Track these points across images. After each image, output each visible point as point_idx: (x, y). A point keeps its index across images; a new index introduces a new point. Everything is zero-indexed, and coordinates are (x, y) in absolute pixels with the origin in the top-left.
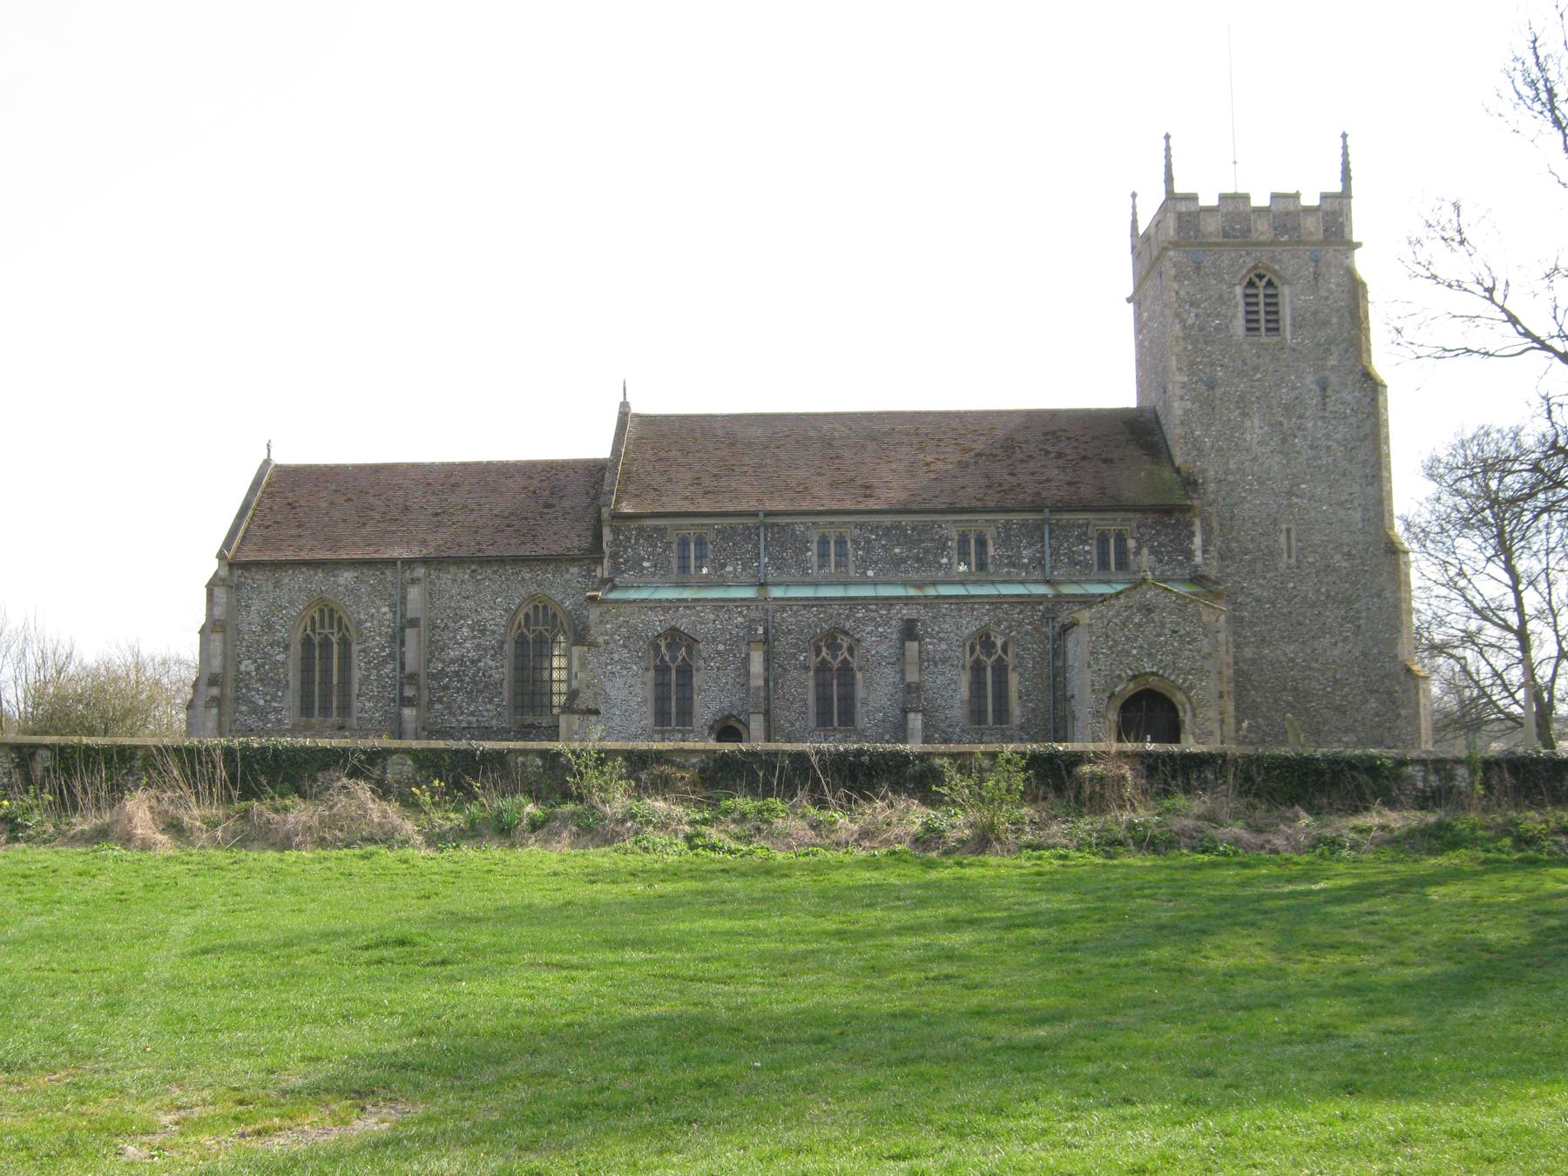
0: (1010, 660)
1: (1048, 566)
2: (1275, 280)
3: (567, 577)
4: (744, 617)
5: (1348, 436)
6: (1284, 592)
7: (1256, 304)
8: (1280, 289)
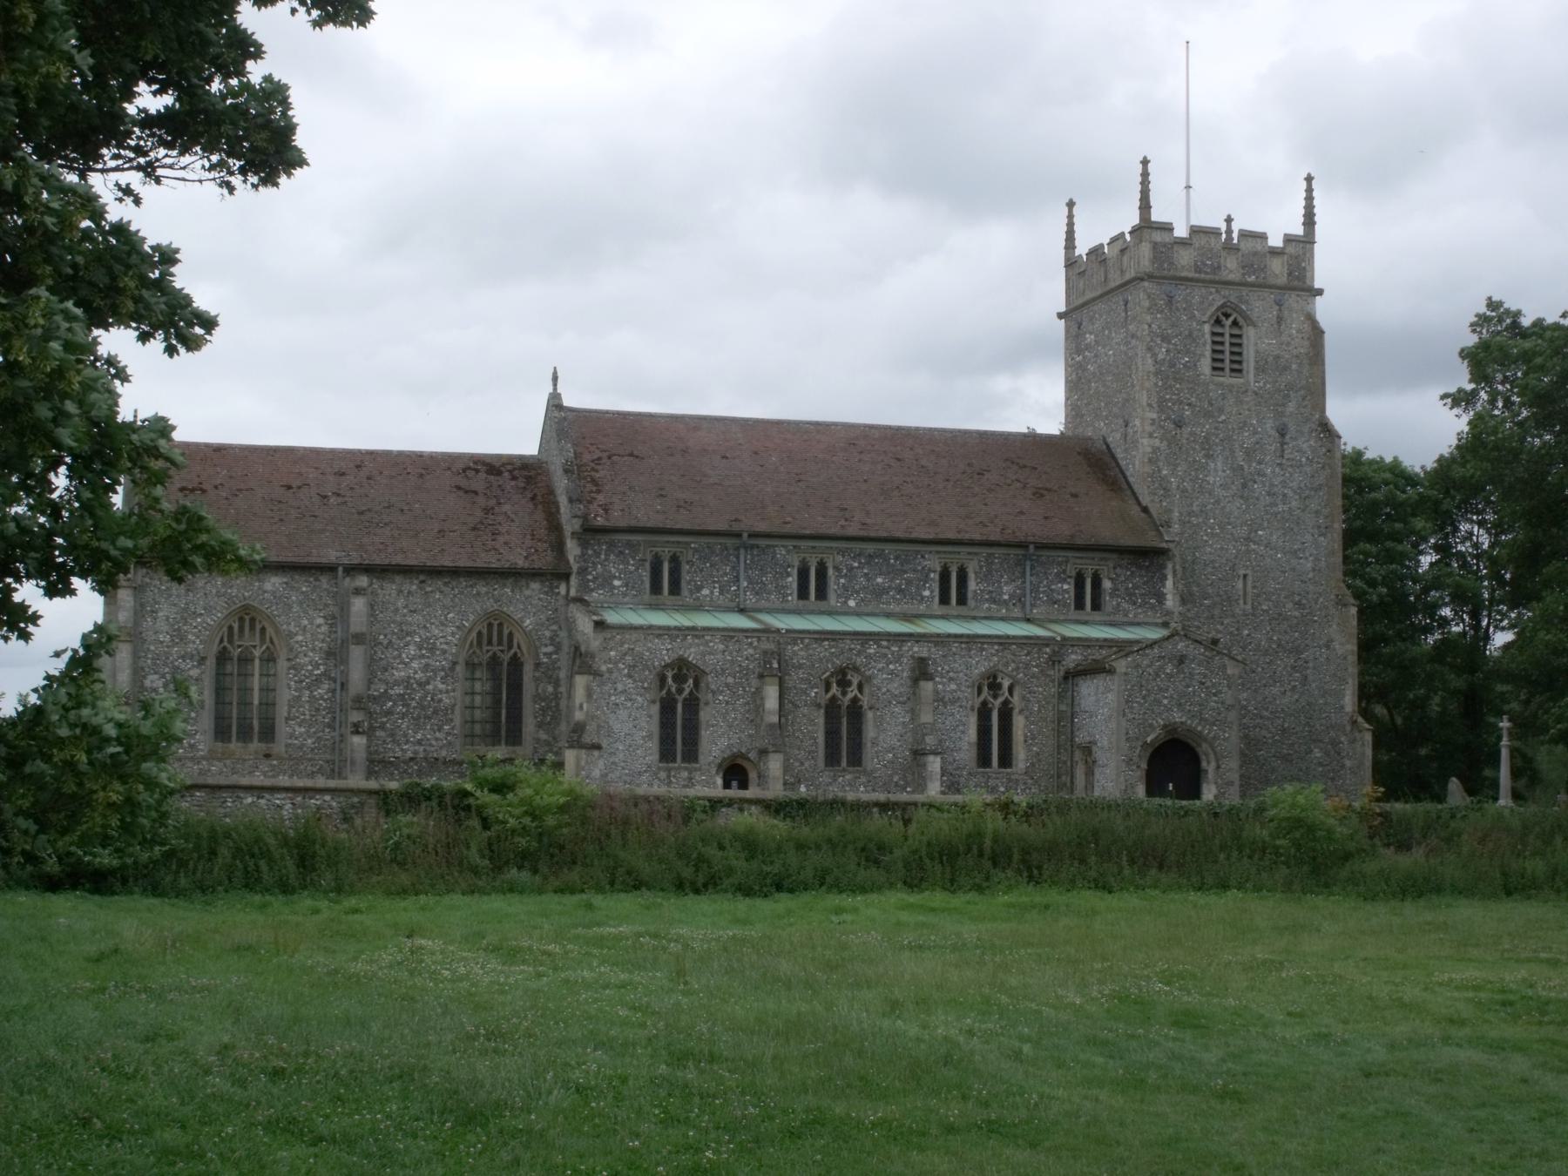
0: (1016, 700)
1: (1028, 603)
2: (1240, 320)
3: (528, 593)
4: (755, 648)
5: (1302, 485)
7: (1222, 343)
8: (1244, 330)
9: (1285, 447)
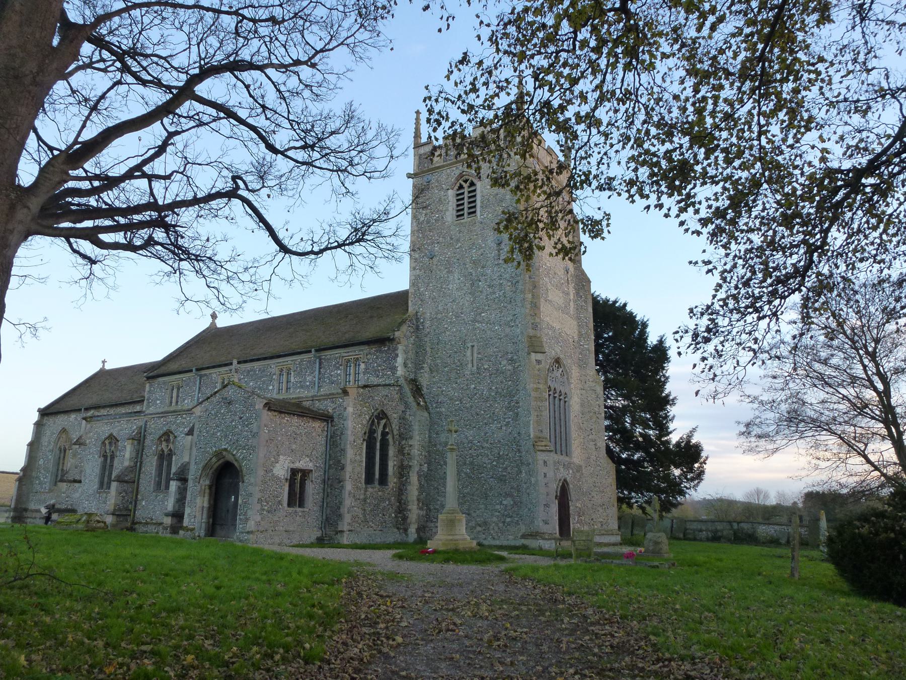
6: (468, 392)
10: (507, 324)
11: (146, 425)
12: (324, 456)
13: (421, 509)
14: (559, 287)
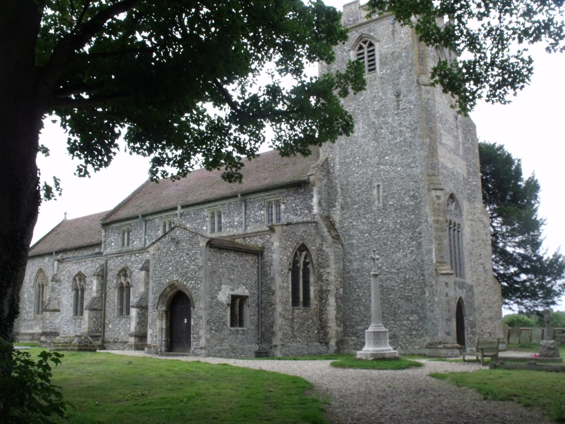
2: (373, 42)
5: (412, 122)
9: (400, 102)
10: (409, 166)
11: (107, 263)
12: (257, 284)
13: (339, 326)
14: (450, 131)
